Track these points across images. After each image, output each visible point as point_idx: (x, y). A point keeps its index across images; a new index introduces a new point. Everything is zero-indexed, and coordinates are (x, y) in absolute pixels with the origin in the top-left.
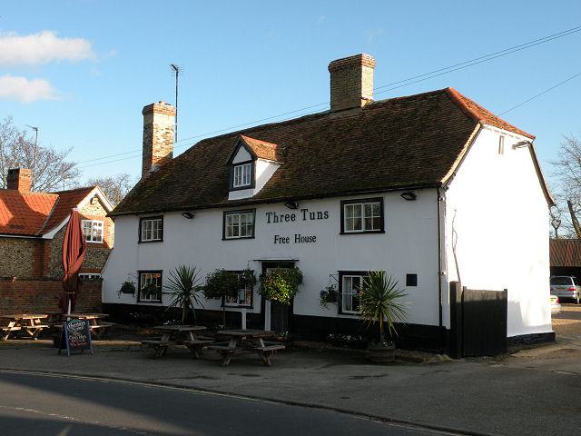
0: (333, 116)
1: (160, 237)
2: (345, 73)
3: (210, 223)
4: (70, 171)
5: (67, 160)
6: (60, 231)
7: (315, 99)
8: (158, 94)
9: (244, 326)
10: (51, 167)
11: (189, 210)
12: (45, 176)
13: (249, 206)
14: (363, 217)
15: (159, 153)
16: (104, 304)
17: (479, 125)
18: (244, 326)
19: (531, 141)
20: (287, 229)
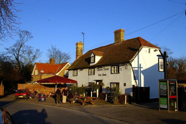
0: (115, 44)
1: (118, 72)
2: (117, 33)
3: (86, 71)
4: (70, 57)
5: (68, 55)
6: (60, 73)
7: (110, 40)
8: (80, 39)
9: (92, 96)
10: (65, 57)
11: (82, 69)
12: (64, 59)
13: (93, 67)
14: (116, 69)
15: (80, 55)
16: (166, 98)
17: (142, 47)
18: (92, 96)
19: (160, 49)
20: (101, 72)
